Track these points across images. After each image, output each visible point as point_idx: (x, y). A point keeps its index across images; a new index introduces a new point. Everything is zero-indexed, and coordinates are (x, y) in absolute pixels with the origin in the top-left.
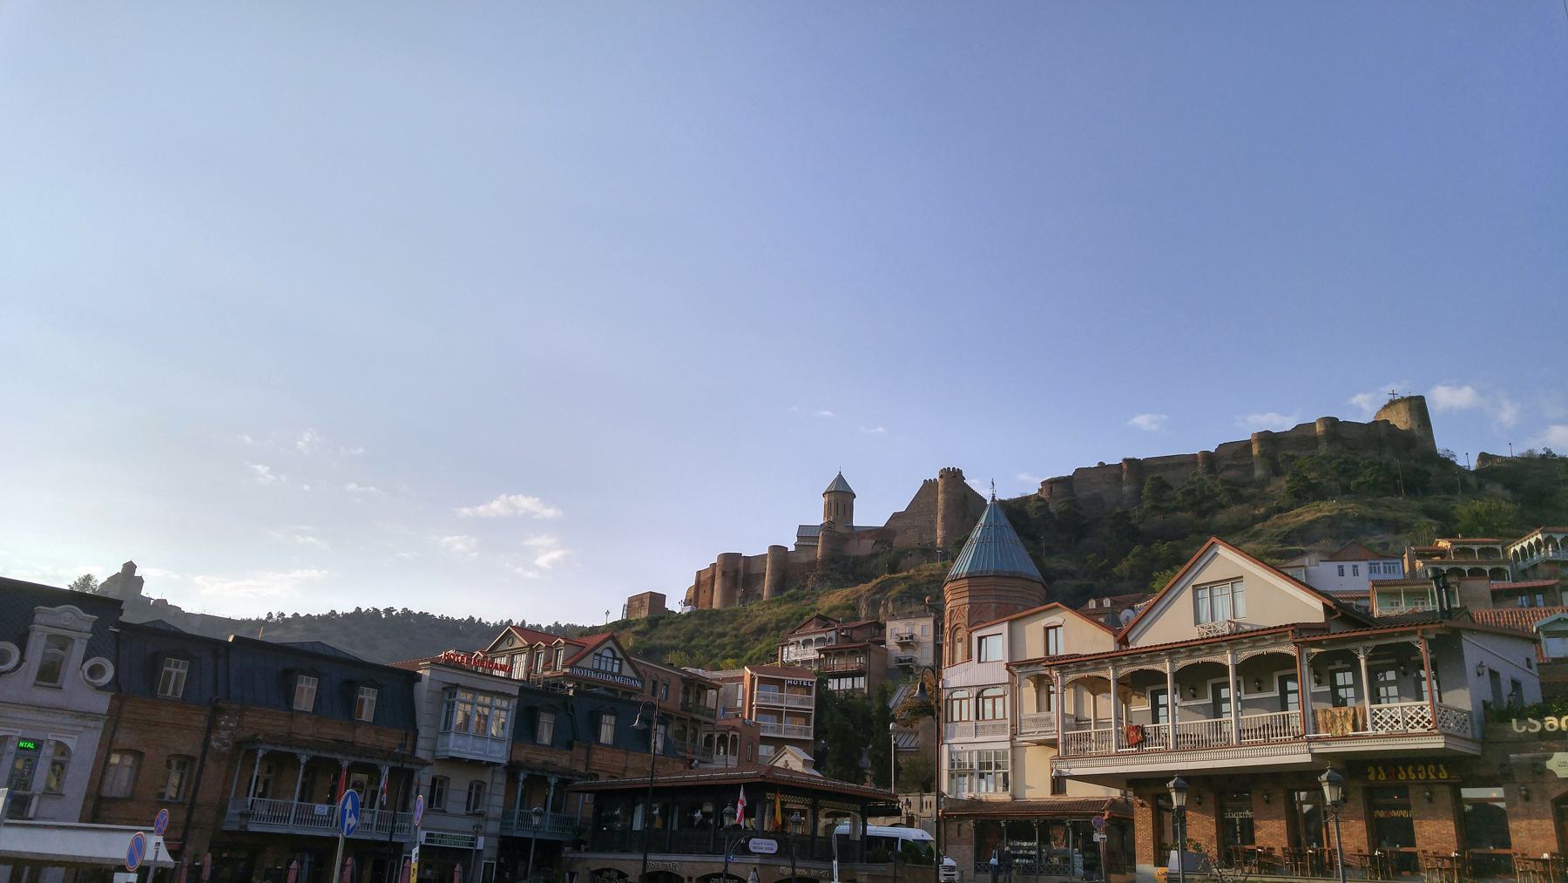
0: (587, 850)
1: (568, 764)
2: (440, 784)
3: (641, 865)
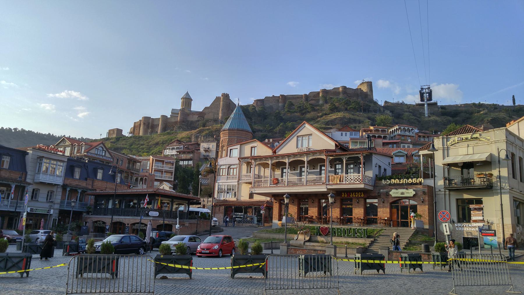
0: (92, 214)
3: (111, 220)
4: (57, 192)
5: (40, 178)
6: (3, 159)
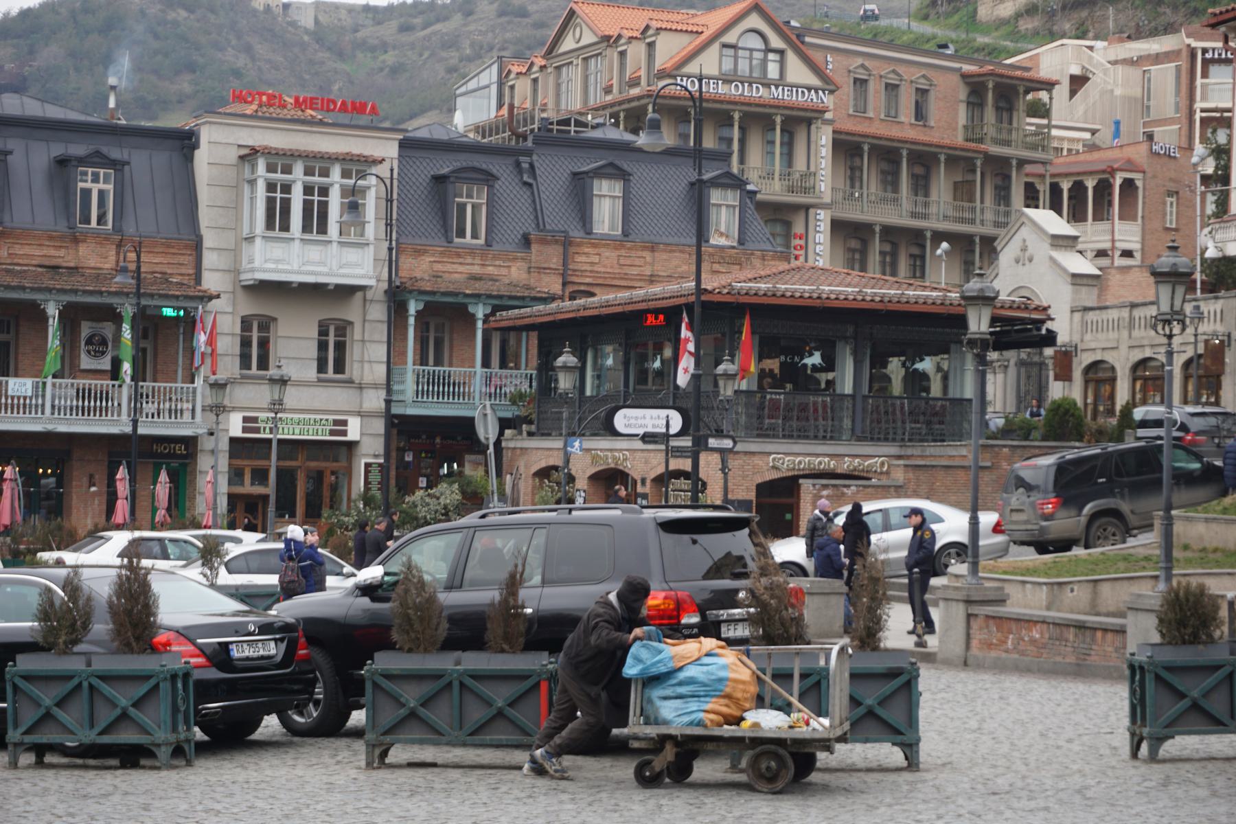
0: (530, 434)
1: (524, 276)
2: (261, 329)
4: (367, 324)
5: (257, 264)
6: (81, 185)
